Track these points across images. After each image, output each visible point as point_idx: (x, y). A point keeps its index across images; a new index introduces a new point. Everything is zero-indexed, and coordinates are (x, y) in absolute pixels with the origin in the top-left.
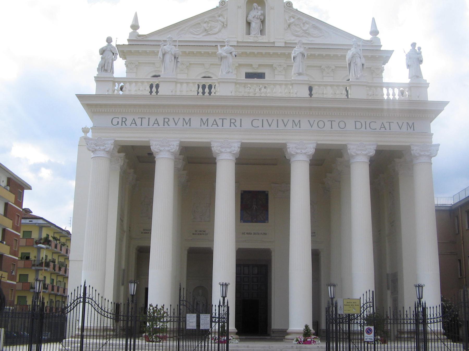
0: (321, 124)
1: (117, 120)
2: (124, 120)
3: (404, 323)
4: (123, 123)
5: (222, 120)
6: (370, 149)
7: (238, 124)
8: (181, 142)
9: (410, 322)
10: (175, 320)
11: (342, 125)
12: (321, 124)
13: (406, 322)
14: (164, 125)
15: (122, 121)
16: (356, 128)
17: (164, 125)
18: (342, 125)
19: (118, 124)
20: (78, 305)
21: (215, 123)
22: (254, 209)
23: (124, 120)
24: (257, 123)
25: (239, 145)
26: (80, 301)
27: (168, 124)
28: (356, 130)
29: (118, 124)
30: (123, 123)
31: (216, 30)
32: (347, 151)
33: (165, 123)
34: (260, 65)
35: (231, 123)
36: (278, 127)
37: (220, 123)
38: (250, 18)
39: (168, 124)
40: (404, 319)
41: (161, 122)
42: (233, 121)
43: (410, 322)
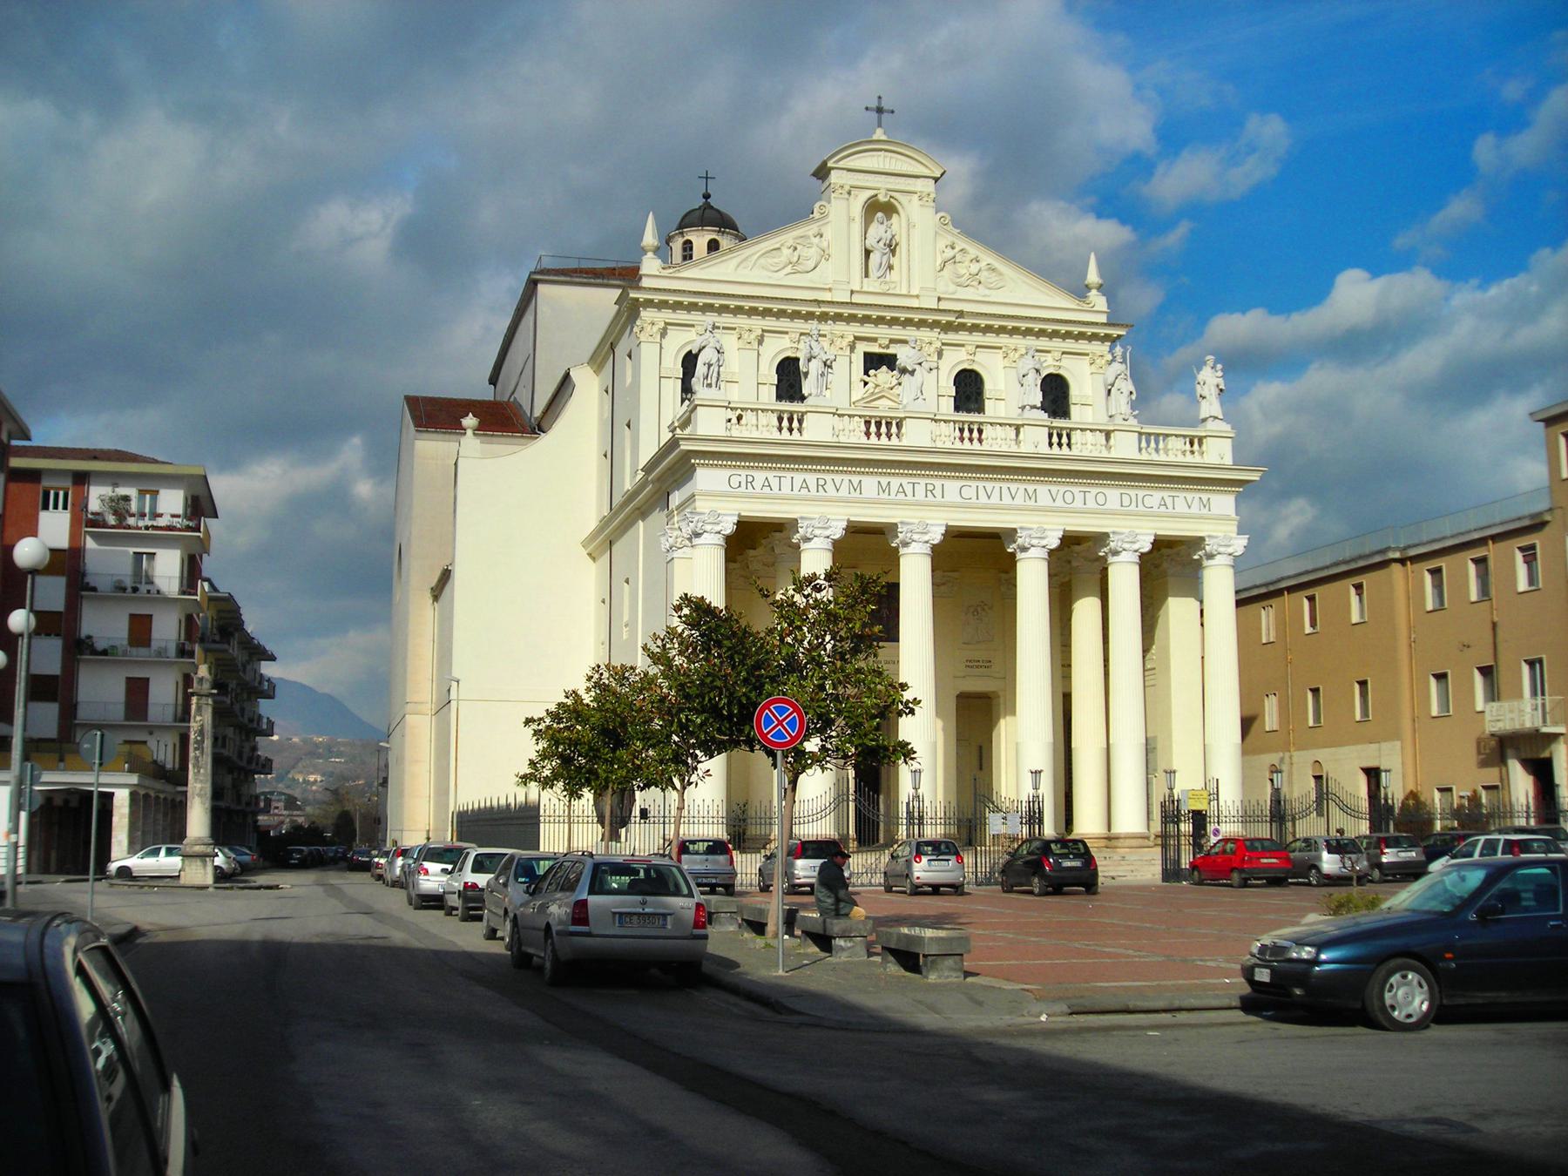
0: (1069, 497)
1: (739, 479)
2: (750, 479)
3: (761, 824)
4: (749, 484)
5: (912, 485)
6: (1144, 541)
7: (938, 492)
8: (849, 521)
9: (654, 821)
10: (1024, 822)
11: (1101, 499)
12: (1069, 497)
13: (763, 823)
14: (818, 491)
15: (747, 482)
16: (1122, 506)
17: (818, 491)
18: (1101, 499)
19: (740, 486)
20: (841, 805)
21: (901, 490)
22: (885, 615)
23: (750, 479)
24: (967, 492)
25: (942, 530)
26: (843, 799)
27: (824, 489)
28: (1122, 508)
29: (740, 486)
30: (749, 484)
31: (811, 264)
32: (636, 319)
33: (820, 487)
34: (892, 341)
35: (927, 490)
36: (1001, 500)
37: (908, 489)
38: (870, 242)
39: (824, 489)
40: (761, 818)
41: (813, 487)
42: (930, 487)
43: (654, 821)
